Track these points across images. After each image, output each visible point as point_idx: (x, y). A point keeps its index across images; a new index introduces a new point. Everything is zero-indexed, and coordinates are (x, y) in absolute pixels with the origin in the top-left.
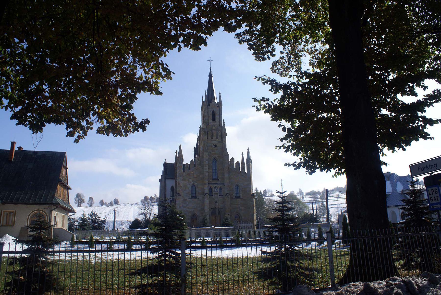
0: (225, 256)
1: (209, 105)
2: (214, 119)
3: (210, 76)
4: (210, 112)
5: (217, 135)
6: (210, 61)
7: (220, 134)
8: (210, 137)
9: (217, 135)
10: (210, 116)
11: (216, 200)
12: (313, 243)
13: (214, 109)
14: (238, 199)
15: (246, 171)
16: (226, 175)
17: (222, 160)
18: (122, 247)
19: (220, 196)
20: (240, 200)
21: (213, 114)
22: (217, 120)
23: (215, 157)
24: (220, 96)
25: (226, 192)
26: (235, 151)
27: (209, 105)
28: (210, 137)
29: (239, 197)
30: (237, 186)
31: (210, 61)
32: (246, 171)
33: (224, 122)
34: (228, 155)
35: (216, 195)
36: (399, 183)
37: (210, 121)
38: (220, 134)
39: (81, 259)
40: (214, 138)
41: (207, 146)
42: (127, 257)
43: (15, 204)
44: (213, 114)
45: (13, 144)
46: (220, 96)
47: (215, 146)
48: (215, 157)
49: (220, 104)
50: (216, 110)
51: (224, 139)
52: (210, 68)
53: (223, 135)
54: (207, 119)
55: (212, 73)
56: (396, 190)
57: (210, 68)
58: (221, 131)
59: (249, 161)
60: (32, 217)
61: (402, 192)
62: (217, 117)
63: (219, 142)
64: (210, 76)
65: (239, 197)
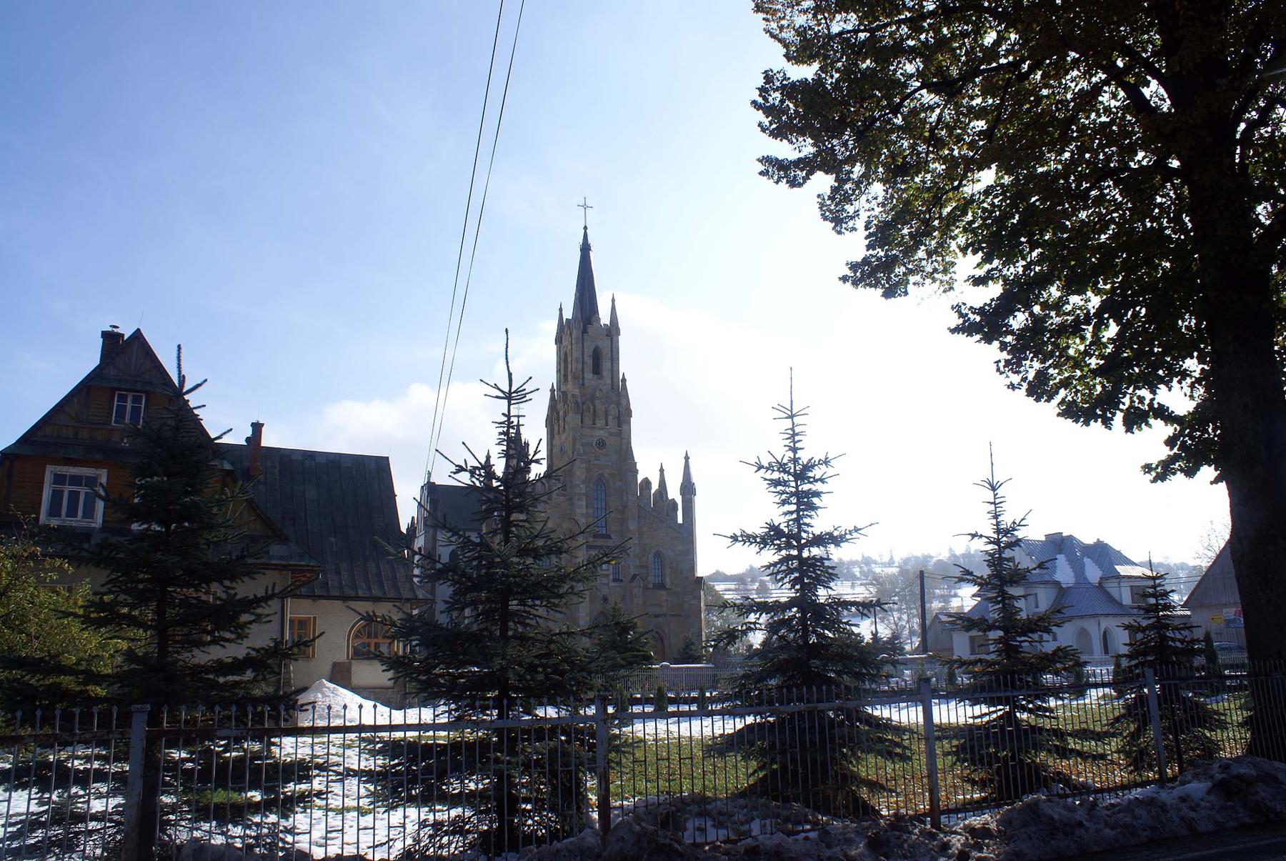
0: (696, 734)
1: (585, 331)
2: (597, 370)
3: (586, 249)
4: (589, 352)
5: (607, 413)
6: (585, 207)
7: (614, 412)
8: (588, 420)
9: (607, 413)
10: (589, 361)
11: (605, 591)
12: (1093, 692)
13: (600, 344)
14: (660, 592)
15: (680, 520)
16: (633, 526)
17: (619, 484)
18: (649, 709)
19: (614, 580)
20: (664, 593)
21: (597, 356)
22: (606, 374)
23: (602, 475)
24: (613, 308)
25: (632, 571)
26: (653, 457)
27: (585, 331)
28: (588, 420)
29: (661, 586)
30: (658, 555)
31: (585, 207)
32: (680, 520)
33: (624, 380)
34: (637, 471)
35: (605, 580)
36: (1087, 561)
37: (589, 375)
38: (614, 412)
39: (696, 734)
40: (600, 423)
41: (583, 444)
42: (685, 731)
43: (313, 597)
44: (597, 356)
45: (257, 427)
46: (613, 308)
47: (601, 444)
48: (602, 475)
49: (612, 331)
50: (604, 344)
51: (624, 427)
52: (585, 228)
53: (623, 415)
54: (580, 366)
55: (590, 241)
56: (1086, 578)
57: (585, 228)
58: (618, 404)
59: (688, 489)
60: (356, 636)
61: (1100, 583)
62: (606, 365)
63: (611, 434)
64: (586, 249)
65: (661, 586)
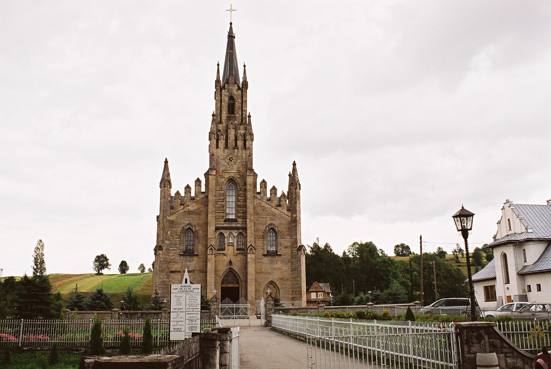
3: (231, 37)
64: (231, 37)
